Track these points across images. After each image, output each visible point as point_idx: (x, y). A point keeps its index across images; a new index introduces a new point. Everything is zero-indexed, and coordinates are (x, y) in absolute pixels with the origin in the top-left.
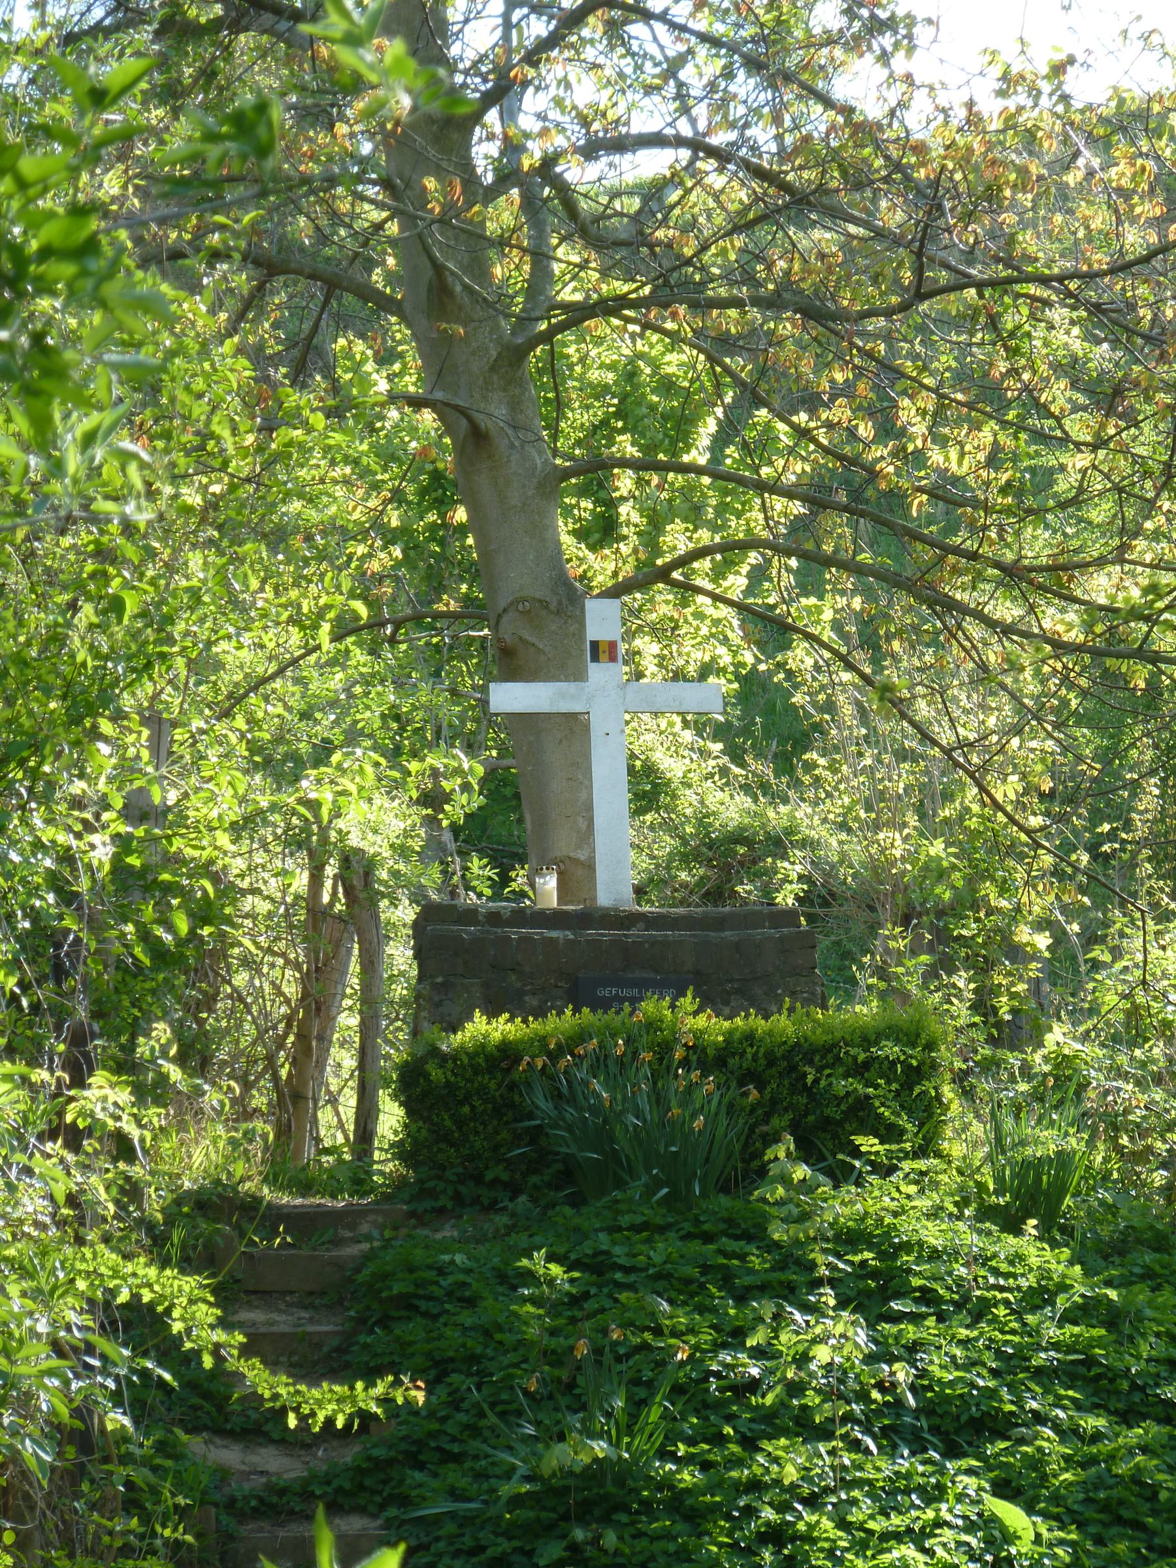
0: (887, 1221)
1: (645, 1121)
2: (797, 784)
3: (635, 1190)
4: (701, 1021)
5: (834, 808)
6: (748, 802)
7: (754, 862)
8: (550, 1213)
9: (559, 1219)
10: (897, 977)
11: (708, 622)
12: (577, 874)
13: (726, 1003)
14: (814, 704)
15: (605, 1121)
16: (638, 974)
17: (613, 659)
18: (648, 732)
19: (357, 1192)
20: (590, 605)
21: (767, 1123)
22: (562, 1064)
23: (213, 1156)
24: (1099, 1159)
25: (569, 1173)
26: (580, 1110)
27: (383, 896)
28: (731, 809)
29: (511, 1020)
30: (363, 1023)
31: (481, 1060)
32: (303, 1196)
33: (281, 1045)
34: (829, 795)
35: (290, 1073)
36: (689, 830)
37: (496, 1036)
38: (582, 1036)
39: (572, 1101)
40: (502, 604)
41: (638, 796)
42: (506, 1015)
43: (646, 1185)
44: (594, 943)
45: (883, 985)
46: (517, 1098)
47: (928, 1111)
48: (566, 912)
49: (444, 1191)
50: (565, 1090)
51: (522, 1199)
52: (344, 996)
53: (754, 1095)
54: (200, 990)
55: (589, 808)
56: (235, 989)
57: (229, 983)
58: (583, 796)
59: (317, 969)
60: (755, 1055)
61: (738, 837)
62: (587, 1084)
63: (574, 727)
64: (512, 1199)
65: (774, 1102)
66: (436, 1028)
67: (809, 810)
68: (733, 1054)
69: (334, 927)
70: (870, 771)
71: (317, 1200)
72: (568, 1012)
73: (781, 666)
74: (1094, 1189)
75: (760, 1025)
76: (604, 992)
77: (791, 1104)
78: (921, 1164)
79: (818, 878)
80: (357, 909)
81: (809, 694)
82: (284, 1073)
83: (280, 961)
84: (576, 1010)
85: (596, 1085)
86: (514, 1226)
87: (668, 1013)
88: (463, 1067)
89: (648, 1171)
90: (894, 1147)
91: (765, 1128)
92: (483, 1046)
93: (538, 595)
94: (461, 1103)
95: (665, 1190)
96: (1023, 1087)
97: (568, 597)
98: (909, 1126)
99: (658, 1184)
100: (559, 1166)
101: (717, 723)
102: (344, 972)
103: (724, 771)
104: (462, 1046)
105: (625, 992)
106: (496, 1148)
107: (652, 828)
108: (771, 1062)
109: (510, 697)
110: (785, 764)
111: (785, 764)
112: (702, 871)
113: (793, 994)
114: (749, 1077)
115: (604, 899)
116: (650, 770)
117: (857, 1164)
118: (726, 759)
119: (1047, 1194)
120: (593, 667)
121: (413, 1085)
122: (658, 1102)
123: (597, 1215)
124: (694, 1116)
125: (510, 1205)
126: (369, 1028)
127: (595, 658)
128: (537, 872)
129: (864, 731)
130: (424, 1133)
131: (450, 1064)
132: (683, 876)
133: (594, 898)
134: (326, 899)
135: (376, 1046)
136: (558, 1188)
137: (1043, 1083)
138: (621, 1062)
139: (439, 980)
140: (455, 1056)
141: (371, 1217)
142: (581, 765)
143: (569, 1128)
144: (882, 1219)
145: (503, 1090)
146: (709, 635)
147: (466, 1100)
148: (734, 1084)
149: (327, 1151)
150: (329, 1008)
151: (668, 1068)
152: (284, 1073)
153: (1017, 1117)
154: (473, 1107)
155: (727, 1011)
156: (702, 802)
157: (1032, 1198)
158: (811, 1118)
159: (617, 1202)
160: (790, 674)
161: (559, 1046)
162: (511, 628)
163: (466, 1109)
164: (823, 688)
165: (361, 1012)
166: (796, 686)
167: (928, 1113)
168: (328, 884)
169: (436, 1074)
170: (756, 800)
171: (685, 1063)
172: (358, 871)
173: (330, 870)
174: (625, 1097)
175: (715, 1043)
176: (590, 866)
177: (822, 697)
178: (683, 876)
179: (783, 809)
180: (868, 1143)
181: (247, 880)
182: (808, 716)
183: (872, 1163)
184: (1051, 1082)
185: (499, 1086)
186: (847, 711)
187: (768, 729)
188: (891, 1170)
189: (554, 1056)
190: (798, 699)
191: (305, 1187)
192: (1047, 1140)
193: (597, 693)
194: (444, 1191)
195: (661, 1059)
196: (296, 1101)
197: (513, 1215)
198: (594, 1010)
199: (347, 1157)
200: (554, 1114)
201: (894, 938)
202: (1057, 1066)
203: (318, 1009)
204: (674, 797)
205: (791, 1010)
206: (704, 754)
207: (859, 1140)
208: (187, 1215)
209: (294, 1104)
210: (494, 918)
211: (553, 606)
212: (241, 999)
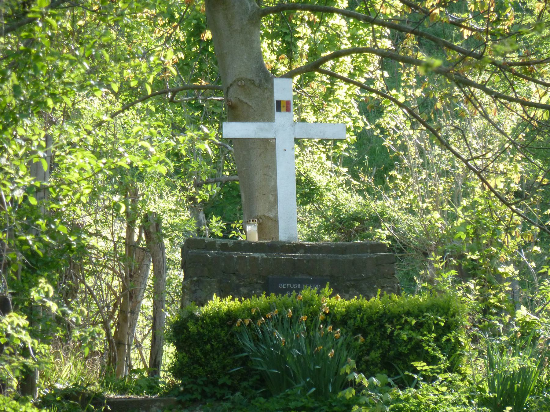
0: (432, 406)
1: (303, 352)
2: (387, 189)
3: (298, 389)
4: (333, 301)
5: (405, 200)
6: (360, 199)
7: (364, 231)
8: (253, 401)
9: (258, 405)
10: (438, 282)
11: (341, 104)
12: (268, 224)
13: (347, 292)
14: (395, 145)
15: (282, 352)
16: (300, 276)
17: (288, 110)
18: (306, 163)
19: (151, 393)
20: (277, 82)
21: (368, 355)
22: (259, 322)
23: (74, 372)
24: (545, 377)
25: (263, 380)
26: (269, 347)
27: (166, 236)
28: (352, 202)
29: (233, 299)
30: (155, 303)
31: (217, 321)
32: (122, 394)
33: (111, 317)
34: (403, 194)
35: (116, 332)
36: (329, 213)
37: (225, 308)
38: (269, 308)
39: (264, 341)
40: (230, 81)
41: (303, 196)
42: (230, 297)
43: (304, 387)
44: (277, 260)
45: (430, 287)
46: (235, 341)
47: (454, 349)
48: (262, 244)
49: (197, 390)
50: (260, 336)
51: (238, 394)
52: (145, 290)
53: (361, 339)
54: (69, 285)
55: (275, 189)
56: (87, 286)
57: (84, 282)
58: (272, 184)
59: (131, 276)
60: (362, 318)
61: (355, 217)
62: (272, 333)
63: (267, 146)
64: (232, 394)
65: (372, 344)
66: (193, 304)
67: (393, 202)
68: (351, 318)
69: (140, 255)
70: (424, 182)
71: (129, 395)
72: (264, 296)
73: (378, 126)
74: (542, 392)
75: (365, 303)
76: (283, 286)
77: (381, 345)
78: (448, 375)
79: (396, 236)
80: (151, 243)
81: (392, 140)
82: (113, 331)
83: (111, 272)
84: (267, 295)
85: (277, 333)
86: (234, 408)
87: (316, 296)
88: (207, 324)
89: (305, 379)
90: (435, 367)
91: (367, 358)
92: (218, 313)
93: (249, 77)
94: (206, 343)
95: (314, 389)
96: (505, 338)
97: (265, 78)
98: (441, 356)
99: (310, 386)
100: (258, 377)
101: (345, 157)
102: (145, 277)
103: (348, 183)
104: (207, 313)
105: (294, 286)
106: (224, 367)
107: (310, 212)
108: (371, 323)
109: (234, 130)
110: (380, 178)
111: (380, 178)
112: (336, 235)
113: (382, 288)
114: (358, 330)
115: (283, 237)
116: (309, 181)
117: (415, 376)
118: (349, 176)
119: (517, 394)
120: (277, 115)
121: (181, 334)
122: (310, 342)
123: (278, 402)
124: (329, 350)
125: (232, 397)
126: (157, 306)
127: (279, 109)
128: (248, 222)
129: (421, 161)
130: (186, 359)
131: (200, 323)
132: (326, 238)
133: (278, 237)
134: (136, 238)
135: (162, 314)
136: (257, 389)
137: (515, 336)
138: (291, 323)
139: (195, 279)
140: (202, 319)
141: (158, 404)
142: (271, 167)
143: (263, 357)
144: (429, 405)
145: (228, 336)
146: (342, 117)
147: (209, 341)
148: (350, 334)
149: (136, 372)
150: (137, 297)
151: (315, 326)
152: (113, 331)
153: (501, 354)
154: (212, 345)
155: (347, 296)
156: (336, 199)
157: (509, 396)
158: (392, 353)
159: (288, 395)
160: (383, 131)
161: (257, 312)
162: (235, 94)
163: (208, 346)
164: (400, 137)
165: (154, 298)
166: (386, 136)
167: (453, 350)
168: (137, 230)
169: (192, 328)
170: (364, 197)
171: (325, 322)
172: (152, 226)
173: (138, 222)
174: (292, 340)
175: (341, 312)
176: (275, 221)
177: (399, 142)
178: (326, 238)
179: (379, 203)
180: (421, 365)
181: (94, 227)
182: (392, 152)
183: (423, 376)
184: (519, 335)
185: (226, 334)
186: (413, 150)
187: (371, 159)
188: (435, 379)
189: (255, 318)
190: (387, 143)
191: (123, 390)
192: (515, 363)
193: (281, 128)
194: (197, 390)
195: (312, 321)
196: (118, 345)
197: (233, 402)
198: (277, 295)
199: (146, 374)
200: (254, 348)
201: (436, 262)
202: (522, 327)
203: (131, 297)
204: (322, 195)
205: (381, 296)
206: (337, 173)
207: (416, 364)
208: (59, 401)
209: (118, 348)
210: (224, 247)
211: (257, 83)
212: (91, 293)
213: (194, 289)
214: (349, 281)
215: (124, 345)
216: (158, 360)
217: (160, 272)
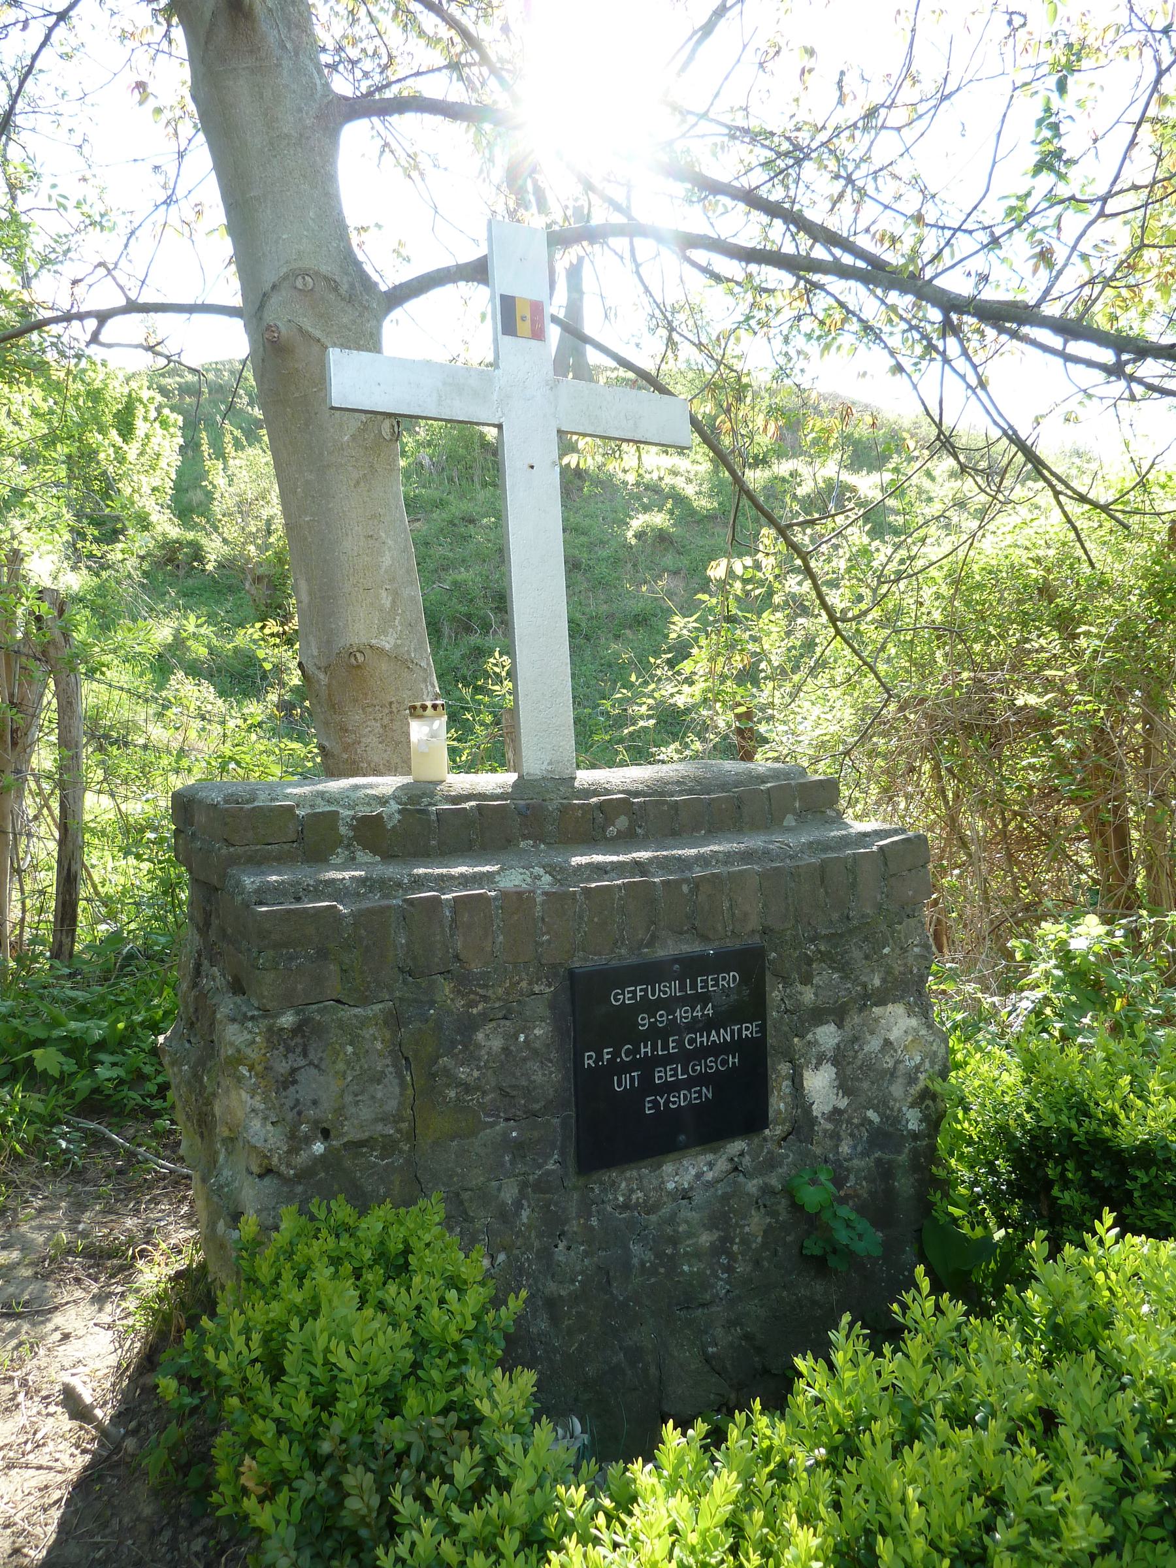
28: (174, 532)
93: (324, 269)
139: (287, 1020)
211: (344, 288)
213: (282, 1067)
214: (812, 940)
215: (6, 833)
216: (73, 870)
217: (71, 703)
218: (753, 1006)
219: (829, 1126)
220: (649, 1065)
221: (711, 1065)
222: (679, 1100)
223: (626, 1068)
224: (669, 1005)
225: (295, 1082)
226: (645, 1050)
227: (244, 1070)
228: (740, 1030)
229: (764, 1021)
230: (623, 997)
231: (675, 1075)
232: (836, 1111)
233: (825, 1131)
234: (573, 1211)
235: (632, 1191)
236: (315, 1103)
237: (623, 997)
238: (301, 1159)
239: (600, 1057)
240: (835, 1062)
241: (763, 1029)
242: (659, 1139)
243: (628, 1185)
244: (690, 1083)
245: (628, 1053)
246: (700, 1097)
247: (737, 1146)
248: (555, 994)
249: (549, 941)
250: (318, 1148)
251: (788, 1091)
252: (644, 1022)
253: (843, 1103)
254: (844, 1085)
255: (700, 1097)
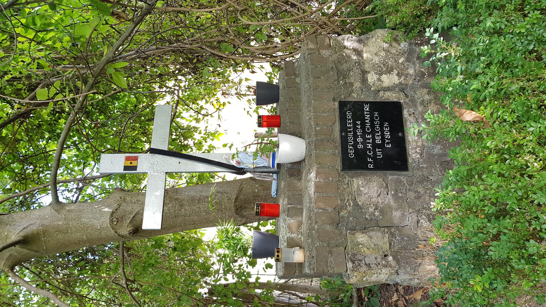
139: (350, 265)
218: (358, 106)
219: (403, 78)
220: (375, 146)
221: (377, 122)
222: (388, 135)
223: (375, 153)
224: (355, 136)
225: (369, 264)
226: (369, 146)
227: (364, 279)
228: (367, 111)
229: (365, 102)
230: (351, 152)
231: (379, 136)
232: (398, 75)
233: (404, 79)
234: (420, 173)
235: (416, 152)
236: (376, 259)
237: (351, 152)
238: (393, 263)
239: (370, 162)
240: (381, 74)
241: (367, 103)
242: (400, 143)
243: (413, 154)
244: (382, 131)
245: (370, 152)
246: (387, 127)
247: (405, 113)
248: (349, 176)
249: (332, 177)
250: (390, 258)
251: (389, 93)
252: (360, 146)
253: (395, 72)
254: (389, 71)
255: (387, 127)
